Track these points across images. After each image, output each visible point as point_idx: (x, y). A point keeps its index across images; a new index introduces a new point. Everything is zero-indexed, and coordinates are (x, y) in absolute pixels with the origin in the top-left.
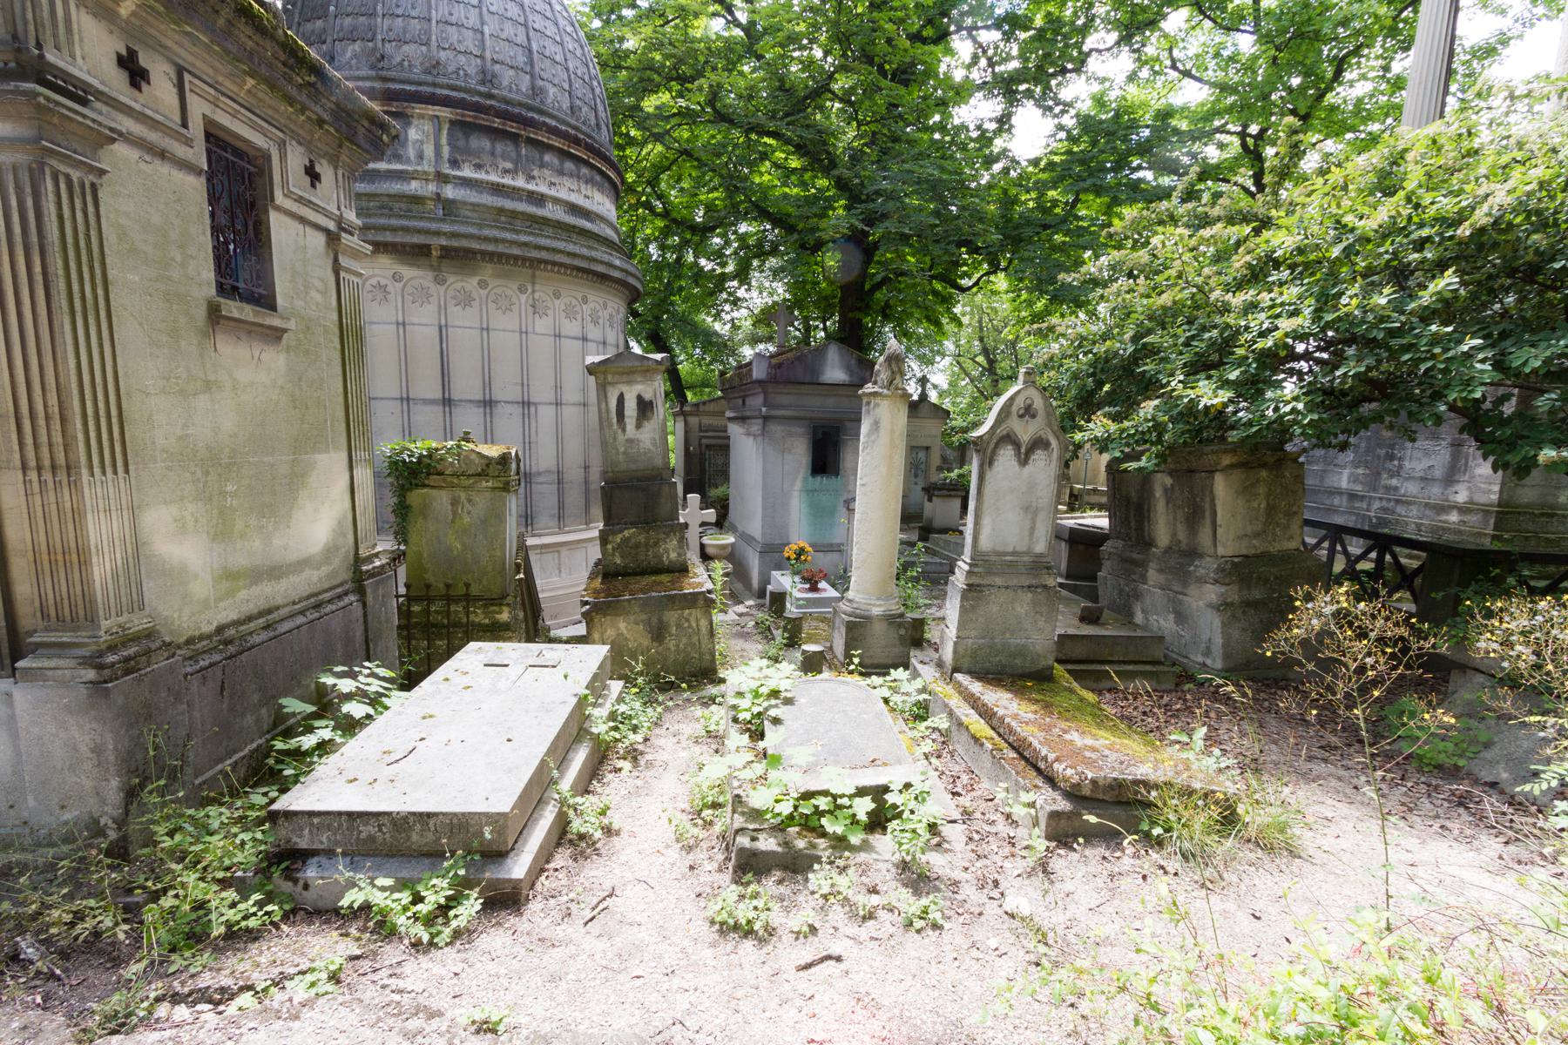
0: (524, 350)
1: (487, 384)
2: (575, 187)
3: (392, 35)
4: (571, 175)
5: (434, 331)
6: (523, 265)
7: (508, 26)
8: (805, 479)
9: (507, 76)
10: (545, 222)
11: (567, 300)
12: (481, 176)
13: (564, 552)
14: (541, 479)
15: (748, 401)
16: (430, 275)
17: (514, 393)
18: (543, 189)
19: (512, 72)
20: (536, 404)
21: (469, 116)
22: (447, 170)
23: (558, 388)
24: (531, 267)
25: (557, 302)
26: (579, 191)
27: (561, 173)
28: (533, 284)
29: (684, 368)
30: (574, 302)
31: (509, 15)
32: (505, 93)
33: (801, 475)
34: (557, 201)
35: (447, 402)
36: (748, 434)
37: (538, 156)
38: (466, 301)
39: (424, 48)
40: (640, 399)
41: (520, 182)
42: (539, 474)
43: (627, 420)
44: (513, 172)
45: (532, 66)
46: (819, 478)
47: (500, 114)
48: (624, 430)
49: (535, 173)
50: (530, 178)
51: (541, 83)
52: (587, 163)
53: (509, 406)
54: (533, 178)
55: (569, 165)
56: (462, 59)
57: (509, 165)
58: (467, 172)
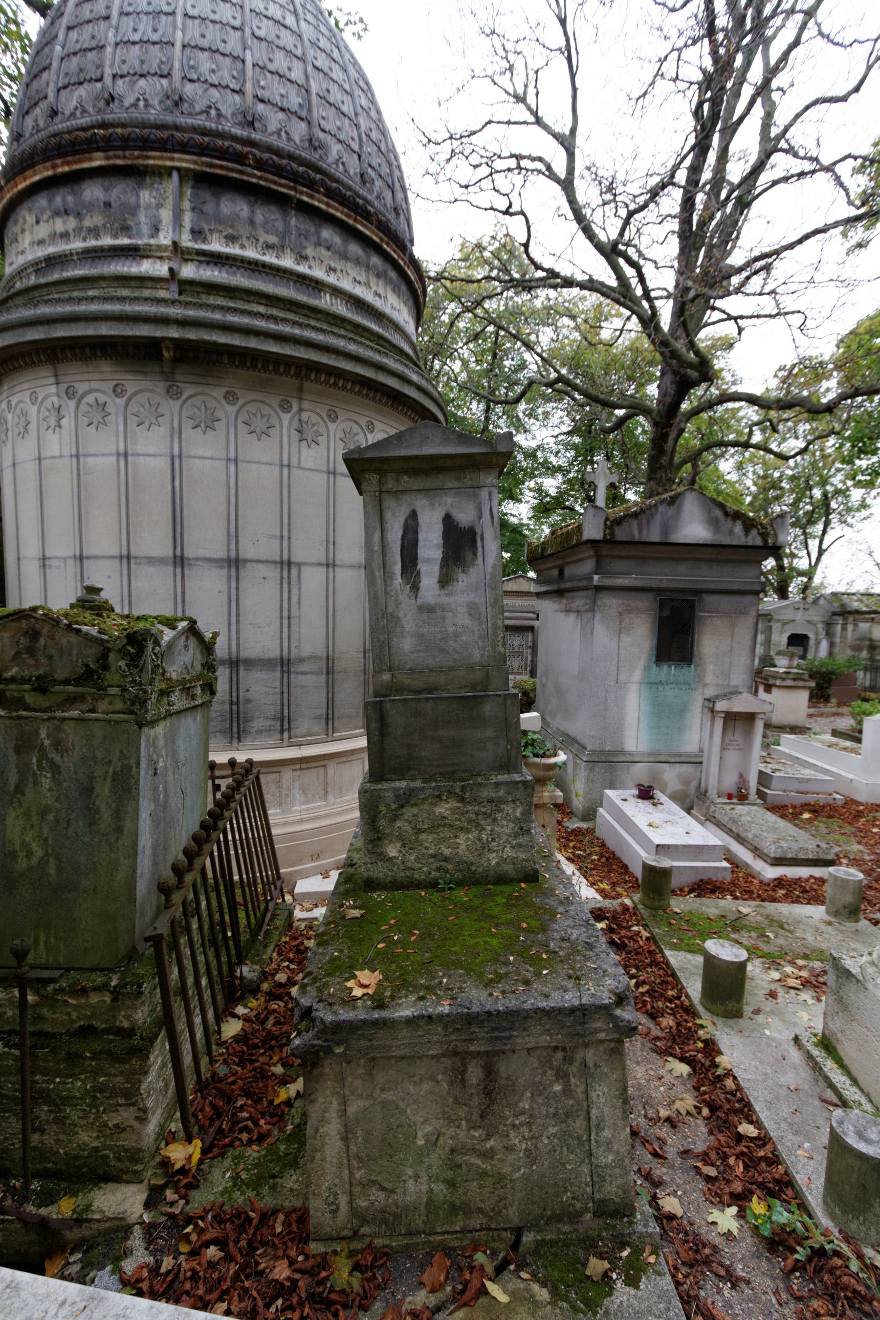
0: (286, 491)
1: (234, 536)
2: (363, 279)
3: (125, 69)
4: (357, 262)
5: (163, 463)
6: (287, 373)
7: (279, 56)
8: (647, 668)
9: (274, 119)
10: (315, 311)
11: (347, 425)
12: (234, 250)
13: (332, 767)
14: (304, 668)
15: (568, 571)
16: (160, 386)
17: (269, 549)
18: (318, 273)
19: (281, 115)
20: (299, 565)
21: (220, 167)
22: (186, 241)
23: (331, 542)
24: (297, 375)
25: (332, 427)
26: (368, 285)
27: (344, 256)
28: (300, 399)
29: (15, 1125)
30: (356, 429)
31: (281, 43)
32: (273, 140)
33: (641, 664)
34: (336, 292)
35: (180, 561)
36: (568, 611)
37: (313, 229)
38: (209, 424)
39: (165, 82)
40: (448, 522)
41: (287, 262)
42: (301, 660)
43: (422, 567)
44: (278, 248)
45: (310, 110)
46: (665, 668)
47: (261, 165)
48: (415, 588)
49: (309, 252)
50: (302, 258)
51: (321, 135)
52: (377, 249)
53: (261, 566)
54: (306, 258)
55: (355, 249)
56: (215, 93)
57: (273, 239)
58: (216, 246)
